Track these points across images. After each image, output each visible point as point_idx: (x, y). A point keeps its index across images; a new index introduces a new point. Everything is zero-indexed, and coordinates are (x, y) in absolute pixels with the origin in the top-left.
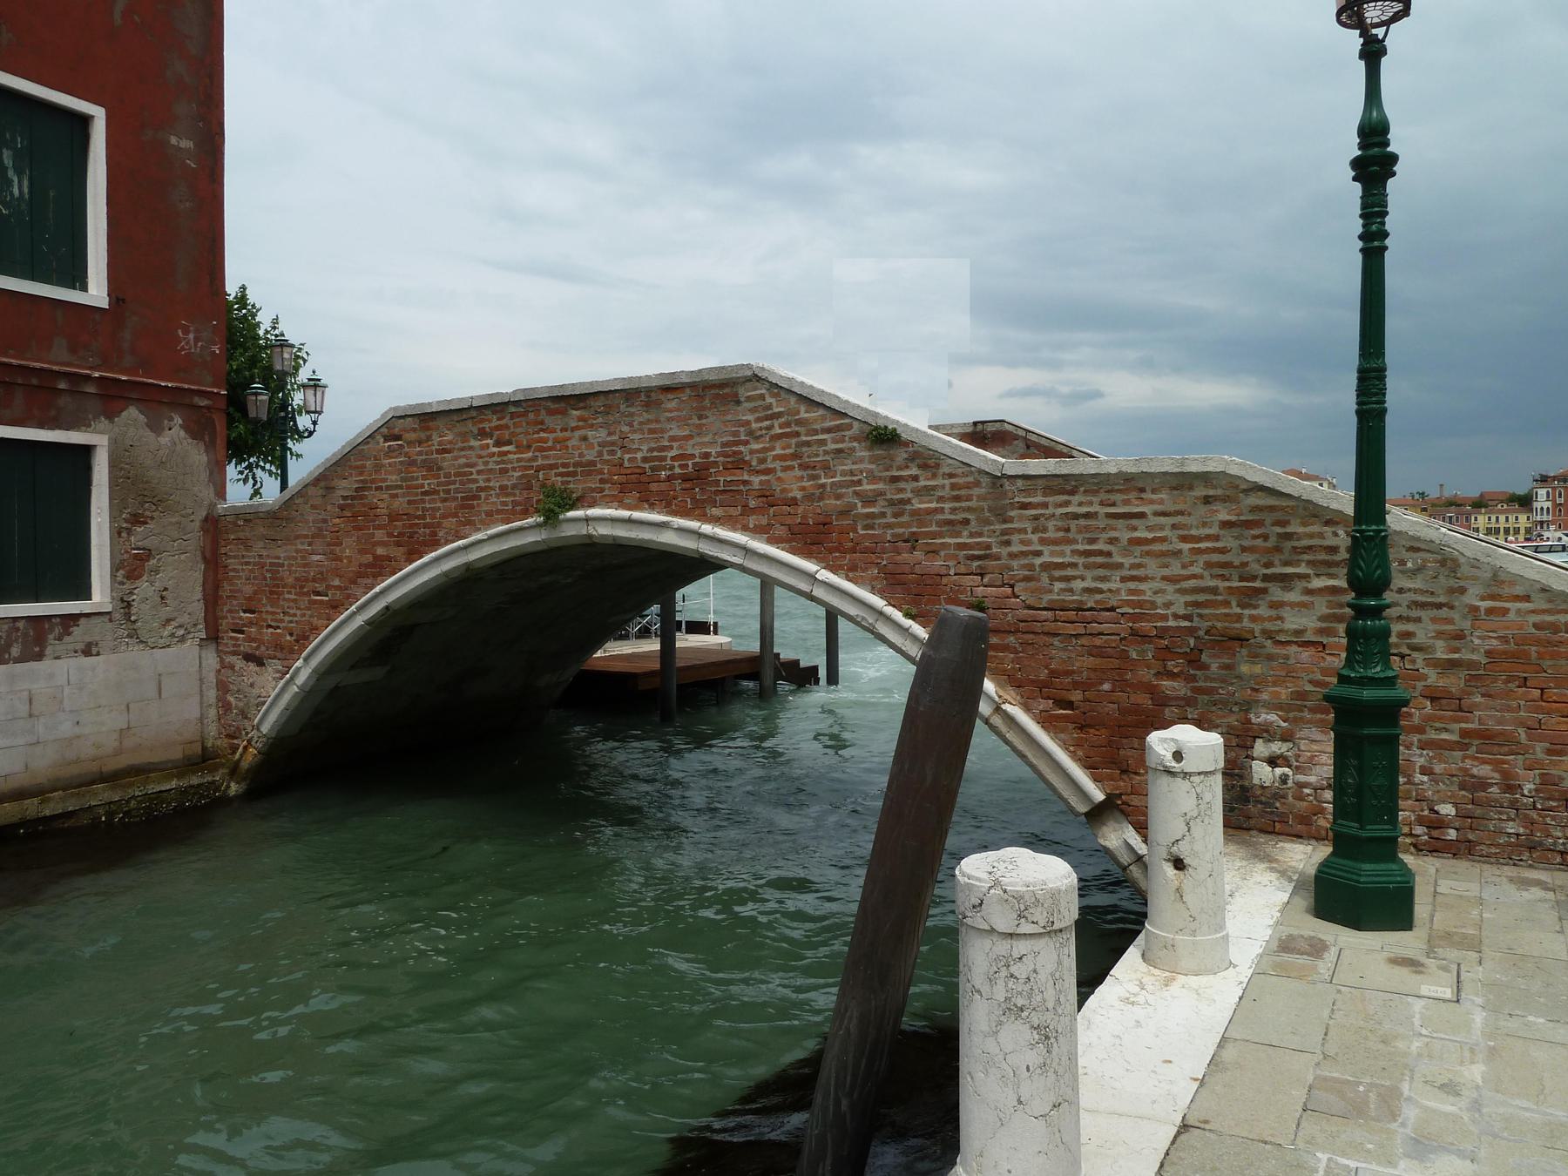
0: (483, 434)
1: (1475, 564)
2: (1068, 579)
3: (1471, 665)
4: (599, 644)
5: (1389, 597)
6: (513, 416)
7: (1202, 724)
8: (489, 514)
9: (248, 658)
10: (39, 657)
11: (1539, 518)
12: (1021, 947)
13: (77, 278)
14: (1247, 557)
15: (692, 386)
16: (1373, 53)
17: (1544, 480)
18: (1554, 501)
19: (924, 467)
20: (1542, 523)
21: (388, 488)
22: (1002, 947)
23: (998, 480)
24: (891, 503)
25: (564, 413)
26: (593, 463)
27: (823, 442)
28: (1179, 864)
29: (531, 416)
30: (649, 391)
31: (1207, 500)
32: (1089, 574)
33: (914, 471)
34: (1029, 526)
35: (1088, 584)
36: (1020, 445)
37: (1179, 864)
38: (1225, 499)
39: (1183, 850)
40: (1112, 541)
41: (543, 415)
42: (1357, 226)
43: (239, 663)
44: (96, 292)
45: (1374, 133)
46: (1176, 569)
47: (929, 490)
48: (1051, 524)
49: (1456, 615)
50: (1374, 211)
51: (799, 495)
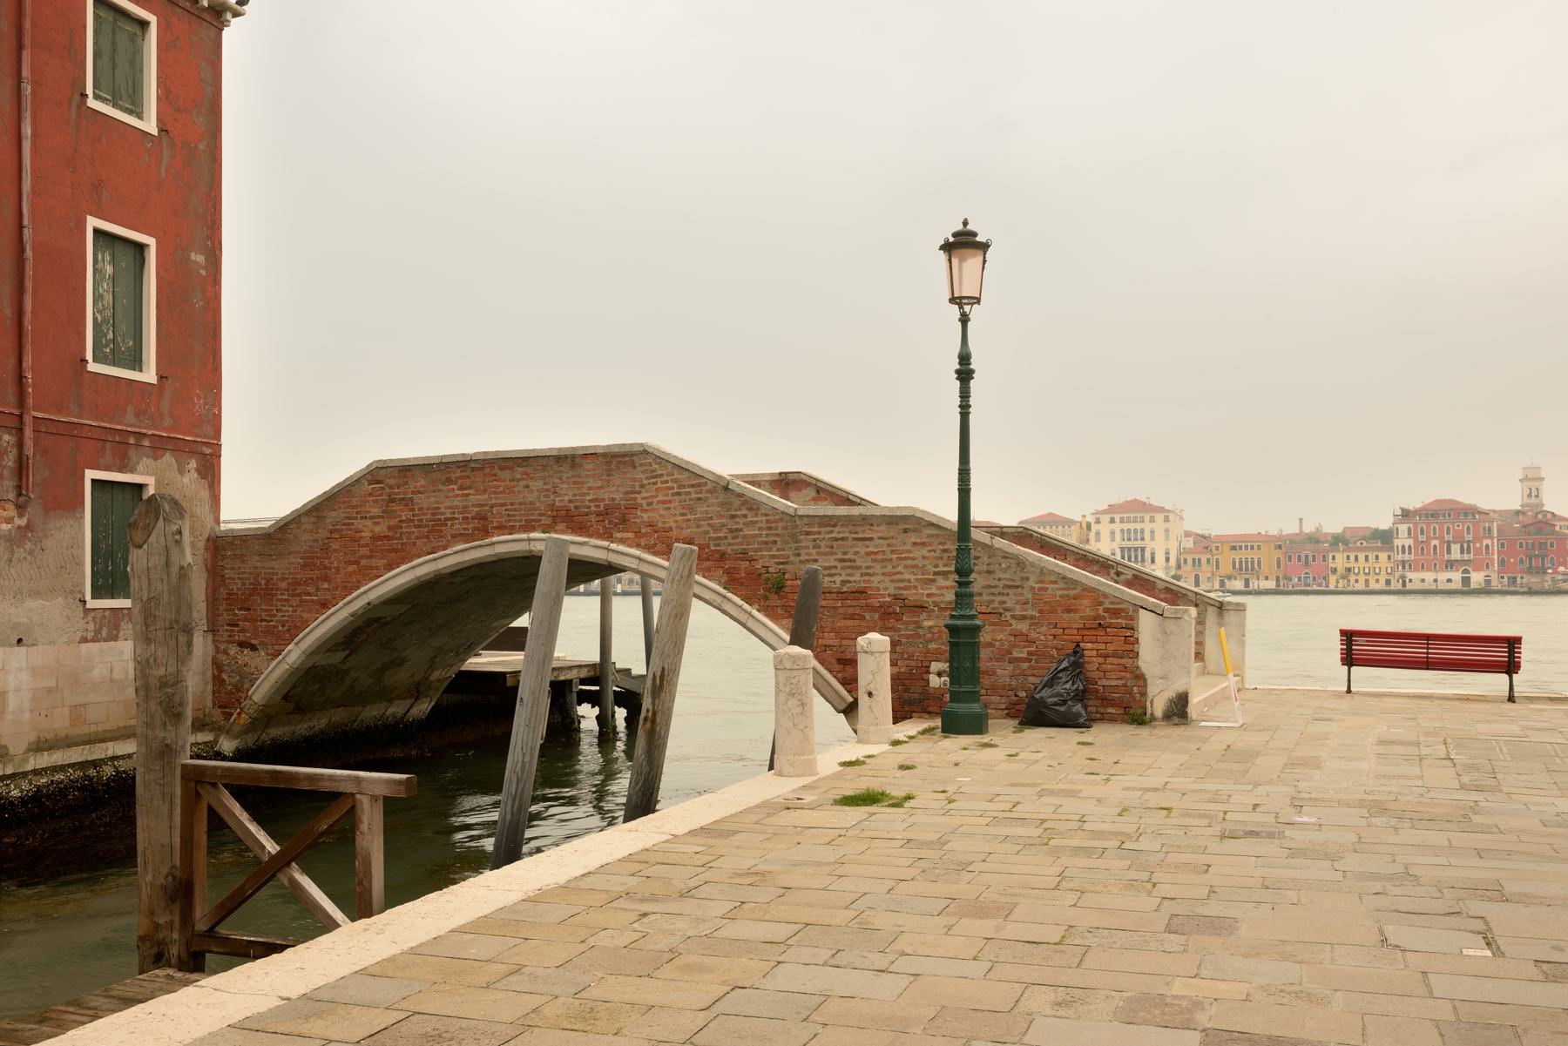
0: (449, 481)
1: (1033, 565)
2: (831, 575)
3: (1033, 617)
4: (470, 649)
5: (973, 577)
6: (473, 469)
7: (881, 632)
8: (454, 536)
9: (242, 645)
10: (115, 638)
11: (1400, 557)
12: (794, 673)
13: (136, 363)
14: (926, 562)
15: (604, 455)
16: (964, 320)
17: (1406, 514)
18: (1416, 538)
19: (750, 509)
20: (1403, 563)
21: (372, 518)
22: (788, 673)
23: (793, 517)
24: (731, 531)
25: (511, 468)
26: (532, 503)
27: (688, 493)
28: (870, 694)
29: (487, 471)
30: (573, 457)
31: (905, 531)
32: (844, 573)
33: (744, 512)
34: (811, 545)
35: (844, 578)
36: (811, 493)
37: (870, 694)
38: (915, 530)
39: (871, 688)
40: (856, 553)
41: (496, 471)
42: (958, 401)
43: (234, 649)
44: (149, 375)
45: (965, 358)
46: (889, 569)
47: (753, 523)
48: (823, 544)
49: (1025, 591)
50: (965, 394)
51: (673, 524)
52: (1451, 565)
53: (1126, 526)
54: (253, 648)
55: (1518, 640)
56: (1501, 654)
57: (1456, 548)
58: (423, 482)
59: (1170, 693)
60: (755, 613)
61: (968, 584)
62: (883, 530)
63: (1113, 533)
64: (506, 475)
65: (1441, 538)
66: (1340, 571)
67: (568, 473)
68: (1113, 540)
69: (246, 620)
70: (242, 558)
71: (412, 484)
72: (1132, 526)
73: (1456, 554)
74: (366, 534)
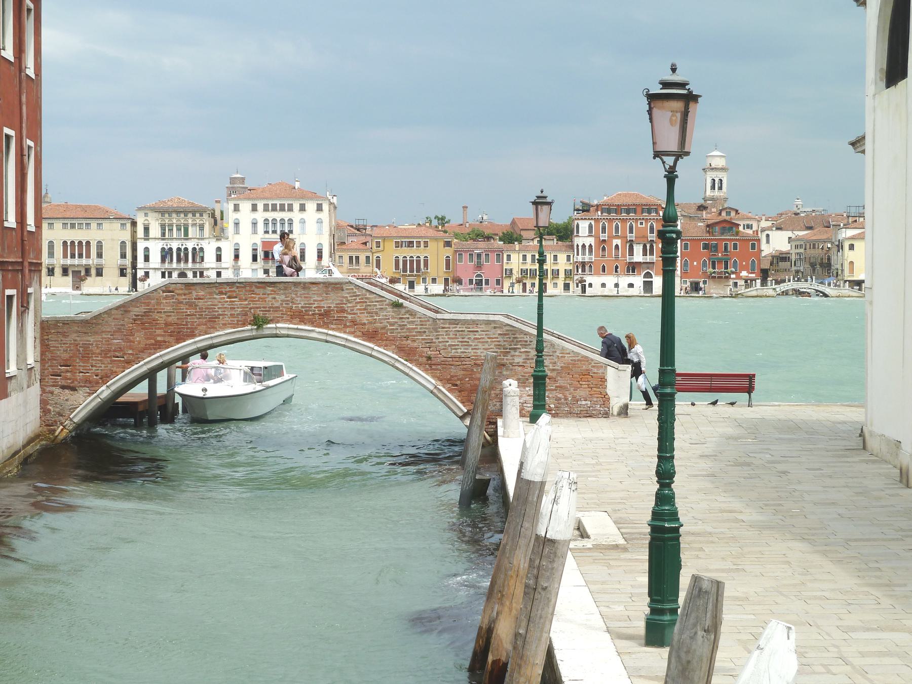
0: (221, 293)
6: (238, 287)
9: (63, 387)
18: (597, 237)
19: (411, 315)
20: (583, 264)
24: (400, 326)
25: (264, 288)
31: (495, 328)
41: (254, 288)
46: (487, 346)
52: (633, 268)
53: (271, 215)
54: (73, 389)
55: (754, 375)
56: (746, 383)
57: (638, 249)
58: (203, 293)
59: (621, 404)
60: (415, 368)
61: (541, 357)
62: (484, 327)
63: (255, 224)
64: (261, 291)
65: (624, 237)
66: (516, 275)
67: (301, 292)
68: (255, 232)
69: (67, 371)
70: (65, 335)
71: (194, 294)
72: (278, 215)
73: (638, 257)
74: (161, 321)
